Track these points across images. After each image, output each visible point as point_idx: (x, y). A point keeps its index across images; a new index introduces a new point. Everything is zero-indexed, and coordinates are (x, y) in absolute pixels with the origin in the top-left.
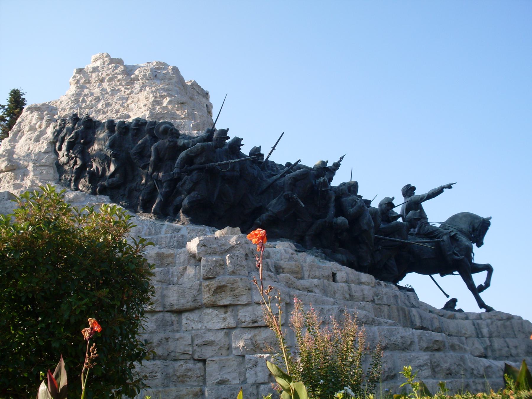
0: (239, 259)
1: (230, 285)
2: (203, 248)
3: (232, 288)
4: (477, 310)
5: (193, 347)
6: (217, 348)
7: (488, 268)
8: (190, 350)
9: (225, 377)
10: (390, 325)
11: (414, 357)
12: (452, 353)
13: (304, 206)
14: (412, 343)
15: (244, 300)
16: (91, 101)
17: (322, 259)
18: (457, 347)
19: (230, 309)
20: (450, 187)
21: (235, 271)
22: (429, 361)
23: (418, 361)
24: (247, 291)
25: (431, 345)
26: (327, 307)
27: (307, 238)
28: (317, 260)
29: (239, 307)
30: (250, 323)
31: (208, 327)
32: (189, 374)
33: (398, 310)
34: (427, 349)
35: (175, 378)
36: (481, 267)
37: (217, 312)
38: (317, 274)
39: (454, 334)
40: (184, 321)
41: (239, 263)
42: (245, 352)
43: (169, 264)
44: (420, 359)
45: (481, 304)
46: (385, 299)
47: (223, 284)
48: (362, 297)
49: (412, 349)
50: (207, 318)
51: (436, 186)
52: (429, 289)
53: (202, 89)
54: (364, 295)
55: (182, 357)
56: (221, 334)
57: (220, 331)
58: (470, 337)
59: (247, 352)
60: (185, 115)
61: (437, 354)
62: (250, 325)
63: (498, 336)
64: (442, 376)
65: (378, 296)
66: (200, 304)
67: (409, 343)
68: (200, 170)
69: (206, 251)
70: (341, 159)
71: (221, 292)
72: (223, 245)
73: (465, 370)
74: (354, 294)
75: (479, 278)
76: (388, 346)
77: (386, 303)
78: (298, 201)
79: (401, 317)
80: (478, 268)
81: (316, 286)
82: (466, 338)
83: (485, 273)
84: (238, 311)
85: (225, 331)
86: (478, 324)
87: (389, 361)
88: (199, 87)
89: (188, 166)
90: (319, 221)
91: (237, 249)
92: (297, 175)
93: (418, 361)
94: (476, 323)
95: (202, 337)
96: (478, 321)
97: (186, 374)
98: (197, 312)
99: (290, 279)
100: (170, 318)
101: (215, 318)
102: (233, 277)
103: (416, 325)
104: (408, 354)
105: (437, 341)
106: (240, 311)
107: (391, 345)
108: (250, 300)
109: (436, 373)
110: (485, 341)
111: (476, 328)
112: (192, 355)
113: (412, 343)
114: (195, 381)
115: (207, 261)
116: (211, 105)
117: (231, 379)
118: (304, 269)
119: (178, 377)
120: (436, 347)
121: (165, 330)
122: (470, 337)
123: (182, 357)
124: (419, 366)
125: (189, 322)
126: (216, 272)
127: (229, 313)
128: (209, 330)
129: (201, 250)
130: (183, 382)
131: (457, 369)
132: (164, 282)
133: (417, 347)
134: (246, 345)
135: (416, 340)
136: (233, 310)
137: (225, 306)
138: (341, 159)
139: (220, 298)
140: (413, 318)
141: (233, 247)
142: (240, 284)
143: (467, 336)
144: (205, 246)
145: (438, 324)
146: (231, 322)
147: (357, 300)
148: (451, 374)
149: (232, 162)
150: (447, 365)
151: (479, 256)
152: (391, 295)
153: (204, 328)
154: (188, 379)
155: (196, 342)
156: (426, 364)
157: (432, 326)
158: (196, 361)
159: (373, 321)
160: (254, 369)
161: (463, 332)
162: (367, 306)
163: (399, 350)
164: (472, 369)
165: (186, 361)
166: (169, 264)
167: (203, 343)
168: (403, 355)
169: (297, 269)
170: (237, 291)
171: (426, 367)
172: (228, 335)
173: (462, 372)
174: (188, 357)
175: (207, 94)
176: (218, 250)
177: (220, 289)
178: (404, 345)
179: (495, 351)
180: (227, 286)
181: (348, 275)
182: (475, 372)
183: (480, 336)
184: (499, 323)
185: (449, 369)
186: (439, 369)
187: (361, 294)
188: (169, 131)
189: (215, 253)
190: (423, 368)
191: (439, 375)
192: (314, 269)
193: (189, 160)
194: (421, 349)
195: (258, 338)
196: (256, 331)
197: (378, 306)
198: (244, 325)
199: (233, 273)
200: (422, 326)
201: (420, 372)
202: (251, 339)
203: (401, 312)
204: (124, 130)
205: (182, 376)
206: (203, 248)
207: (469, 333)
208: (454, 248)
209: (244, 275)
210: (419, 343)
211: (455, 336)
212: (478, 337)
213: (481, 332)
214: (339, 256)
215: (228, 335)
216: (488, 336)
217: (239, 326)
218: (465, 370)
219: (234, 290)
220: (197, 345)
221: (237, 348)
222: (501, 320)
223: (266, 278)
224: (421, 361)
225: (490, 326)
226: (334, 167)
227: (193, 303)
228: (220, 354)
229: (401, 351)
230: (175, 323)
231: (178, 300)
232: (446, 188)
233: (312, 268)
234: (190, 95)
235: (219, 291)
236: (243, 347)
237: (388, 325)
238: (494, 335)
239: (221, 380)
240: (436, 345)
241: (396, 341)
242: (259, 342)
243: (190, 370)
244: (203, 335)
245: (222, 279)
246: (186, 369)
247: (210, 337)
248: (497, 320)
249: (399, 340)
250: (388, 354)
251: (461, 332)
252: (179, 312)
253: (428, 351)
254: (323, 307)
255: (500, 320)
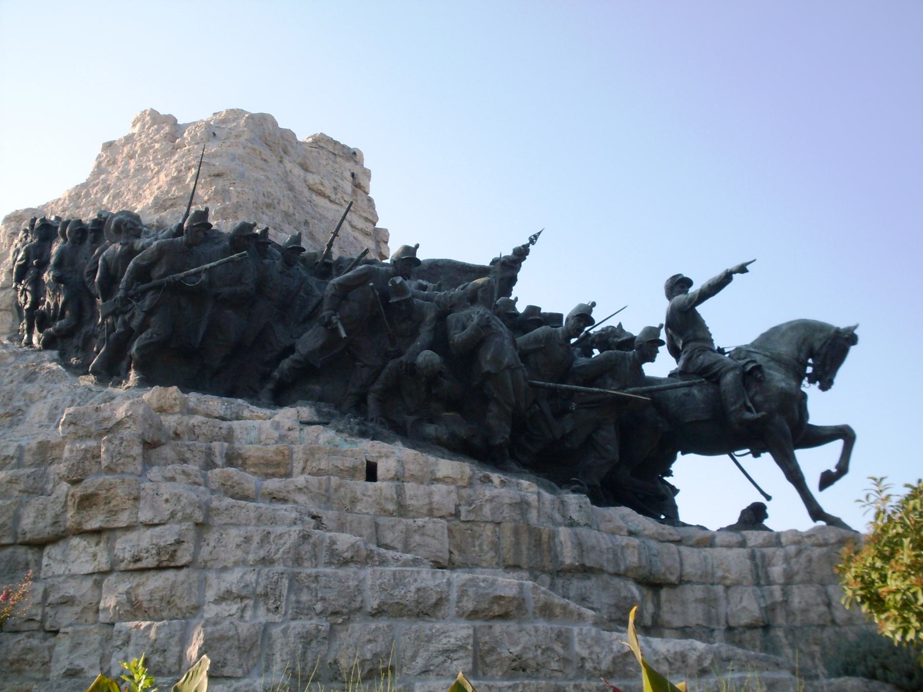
0: (125, 443)
1: (103, 493)
2: (72, 428)
3: (106, 498)
4: (804, 523)
5: (44, 607)
6: (78, 609)
7: (846, 435)
8: (38, 613)
9: (76, 663)
10: (405, 564)
11: (438, 630)
12: (542, 624)
13: (344, 335)
14: (440, 603)
15: (123, 519)
16: (96, 194)
17: (351, 435)
18: (558, 611)
19: (105, 536)
20: (742, 269)
21: (112, 466)
22: (471, 641)
23: (444, 641)
24: (131, 502)
25: (485, 605)
26: (280, 529)
27: (371, 398)
28: (338, 439)
29: (118, 533)
30: (130, 562)
31: (72, 572)
32: (29, 657)
33: (516, 532)
34: (473, 615)
35: (7, 664)
36: (828, 432)
37: (85, 543)
38: (323, 465)
39: (694, 579)
40: (45, 561)
41: (122, 451)
42: (117, 617)
43: (54, 460)
44: (450, 636)
45: (816, 512)
46: (487, 510)
47: (90, 491)
48: (428, 507)
49: (440, 614)
50: (73, 554)
51: (716, 272)
52: (708, 488)
53: (344, 146)
54: (431, 503)
55: (26, 627)
56: (89, 583)
57: (89, 577)
58: (738, 583)
59: (121, 618)
60: (209, 196)
61: (499, 627)
62: (131, 566)
63: (809, 582)
64: (500, 673)
65: (470, 505)
66: (62, 529)
67: (433, 600)
68: (158, 288)
69: (75, 433)
70: (533, 240)
71: (91, 507)
72: (105, 419)
73: (566, 661)
74: (408, 502)
75: (814, 461)
76: (385, 608)
77: (490, 519)
78: (337, 328)
79: (524, 548)
80: (820, 437)
81: (300, 489)
82: (727, 588)
83: (839, 444)
84: (115, 540)
85: (95, 577)
86: (763, 556)
87: (380, 639)
88: (336, 143)
89: (138, 285)
90: (391, 364)
91: (127, 426)
92: (348, 278)
93: (444, 641)
94: (758, 554)
95: (59, 589)
96: (765, 550)
97: (24, 657)
98: (61, 543)
99: (230, 477)
100: (24, 556)
101: (82, 555)
102: (110, 478)
103: (562, 563)
104: (428, 625)
105: (501, 598)
106: (119, 541)
107: (391, 605)
108: (135, 520)
109: (487, 666)
110: (771, 594)
111: (756, 566)
112: (42, 622)
113: (440, 603)
114: (39, 670)
115: (71, 451)
116: (367, 174)
117: (86, 668)
118: (295, 456)
119: (12, 664)
120: (496, 609)
121: (13, 578)
122: (738, 583)
123: (26, 627)
124: (447, 651)
125: (51, 562)
126: (83, 470)
127: (102, 545)
128: (73, 576)
129: (67, 431)
130: (20, 672)
131: (541, 659)
132: (33, 493)
133: (453, 610)
134: (118, 603)
135: (454, 596)
136: (108, 539)
137: (98, 532)
138: (533, 240)
139: (88, 518)
140: (559, 549)
141: (120, 423)
142: (119, 491)
143: (728, 582)
144: (75, 424)
145: (635, 560)
146: (103, 562)
147: (414, 514)
148: (524, 670)
149: (206, 269)
150: (516, 650)
151: (822, 407)
152: (507, 501)
153: (67, 572)
154: (27, 668)
155: (51, 599)
156: (462, 647)
157: (617, 564)
158: (49, 634)
159: (370, 556)
160: (125, 648)
161: (719, 573)
162: (431, 525)
163: (409, 616)
164: (583, 659)
165: (31, 634)
166: (54, 460)
167: (59, 601)
168: (415, 627)
169: (279, 458)
170: (114, 503)
171: (461, 653)
172: (98, 585)
173: (554, 665)
174: (35, 626)
175: (355, 153)
176: (93, 429)
177: (86, 502)
178: (421, 606)
179: (793, 614)
180: (97, 495)
181: (402, 466)
182: (589, 665)
183: (762, 582)
184: (817, 551)
185: (519, 657)
186: (494, 657)
187: (427, 501)
188: (122, 227)
189: (88, 436)
190: (455, 656)
191: (494, 671)
192: (317, 456)
193: (143, 274)
194: (460, 615)
195: (141, 590)
196: (143, 578)
197: (468, 525)
198: (123, 566)
199: (110, 470)
200: (583, 565)
201: (447, 664)
202: (128, 593)
203: (525, 538)
204: (80, 235)
205: (18, 661)
206: (72, 426)
207: (732, 577)
208: (762, 401)
209: (132, 473)
210: (458, 602)
211: (698, 583)
212: (758, 584)
213: (766, 573)
214: (430, 430)
215: (98, 585)
216: (782, 581)
217: (117, 568)
218: (566, 661)
219: (110, 502)
220: (49, 604)
221: (106, 609)
222: (826, 544)
223: (178, 477)
224: (453, 641)
225: (793, 561)
226: (516, 258)
227: (53, 529)
228: (83, 620)
229: (413, 619)
230: (32, 564)
231: (34, 523)
232: (735, 272)
233: (312, 454)
234: (299, 160)
235: (86, 503)
236: (115, 607)
237: (399, 563)
238: (797, 578)
239: (68, 670)
240: (499, 604)
241: (403, 597)
242: (141, 598)
243: (31, 650)
244: (61, 586)
245: (91, 484)
246: (23, 649)
247: (71, 589)
248: (813, 545)
249: (411, 596)
250: (381, 625)
251: (713, 574)
252: (39, 545)
253: (479, 618)
254: (271, 530)
255: (820, 545)
